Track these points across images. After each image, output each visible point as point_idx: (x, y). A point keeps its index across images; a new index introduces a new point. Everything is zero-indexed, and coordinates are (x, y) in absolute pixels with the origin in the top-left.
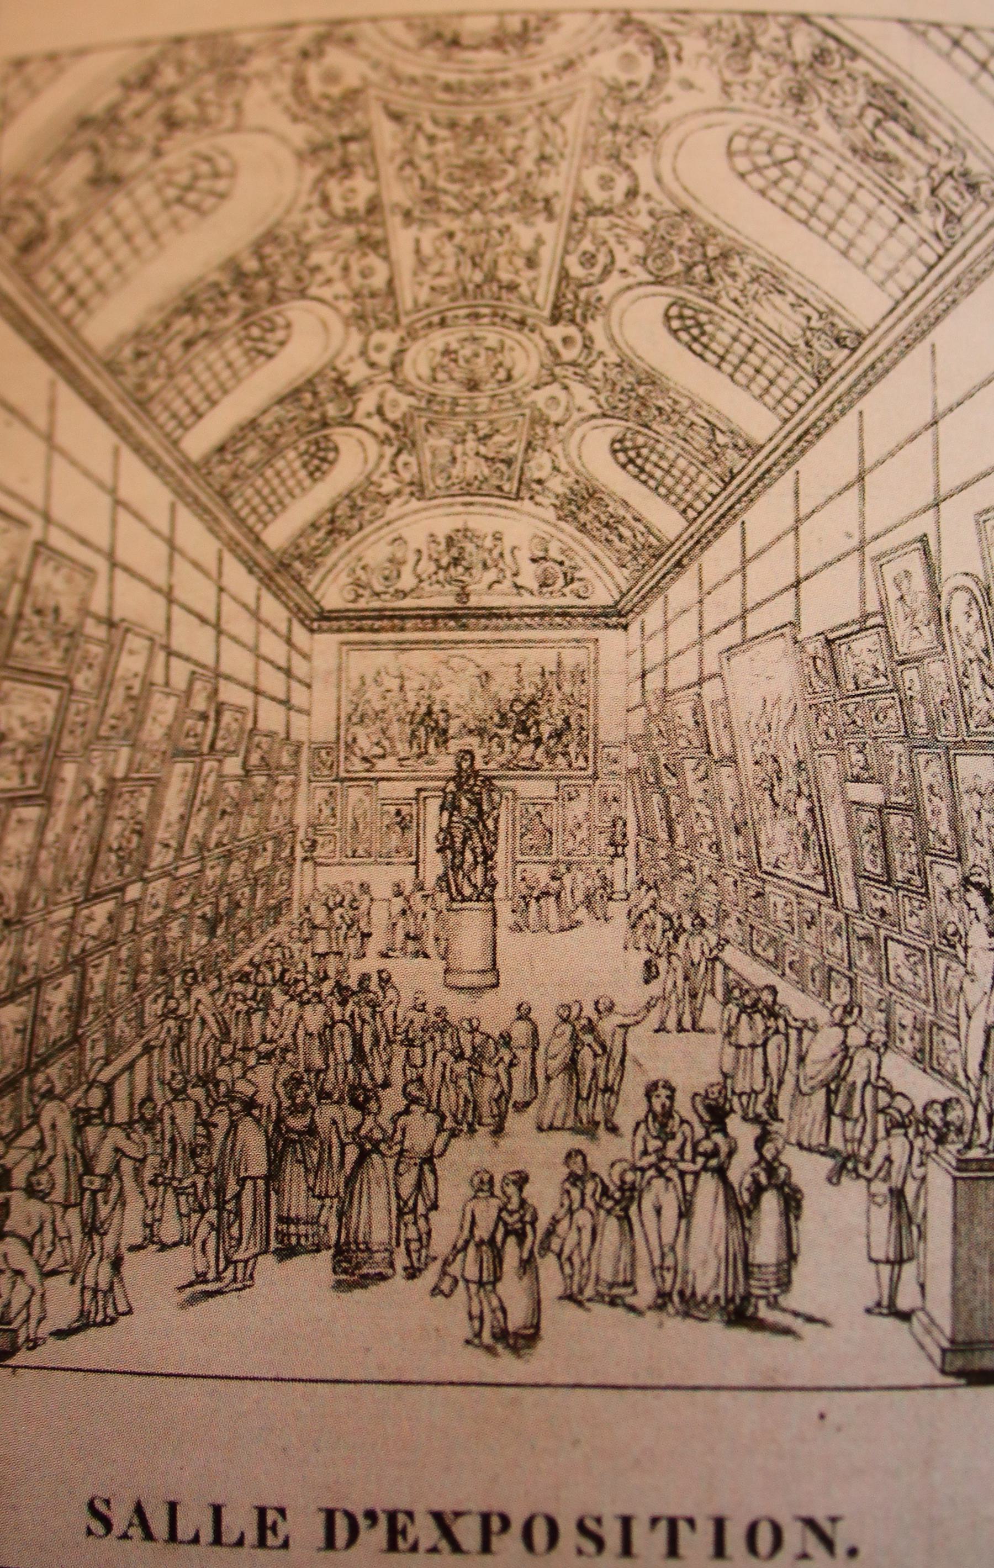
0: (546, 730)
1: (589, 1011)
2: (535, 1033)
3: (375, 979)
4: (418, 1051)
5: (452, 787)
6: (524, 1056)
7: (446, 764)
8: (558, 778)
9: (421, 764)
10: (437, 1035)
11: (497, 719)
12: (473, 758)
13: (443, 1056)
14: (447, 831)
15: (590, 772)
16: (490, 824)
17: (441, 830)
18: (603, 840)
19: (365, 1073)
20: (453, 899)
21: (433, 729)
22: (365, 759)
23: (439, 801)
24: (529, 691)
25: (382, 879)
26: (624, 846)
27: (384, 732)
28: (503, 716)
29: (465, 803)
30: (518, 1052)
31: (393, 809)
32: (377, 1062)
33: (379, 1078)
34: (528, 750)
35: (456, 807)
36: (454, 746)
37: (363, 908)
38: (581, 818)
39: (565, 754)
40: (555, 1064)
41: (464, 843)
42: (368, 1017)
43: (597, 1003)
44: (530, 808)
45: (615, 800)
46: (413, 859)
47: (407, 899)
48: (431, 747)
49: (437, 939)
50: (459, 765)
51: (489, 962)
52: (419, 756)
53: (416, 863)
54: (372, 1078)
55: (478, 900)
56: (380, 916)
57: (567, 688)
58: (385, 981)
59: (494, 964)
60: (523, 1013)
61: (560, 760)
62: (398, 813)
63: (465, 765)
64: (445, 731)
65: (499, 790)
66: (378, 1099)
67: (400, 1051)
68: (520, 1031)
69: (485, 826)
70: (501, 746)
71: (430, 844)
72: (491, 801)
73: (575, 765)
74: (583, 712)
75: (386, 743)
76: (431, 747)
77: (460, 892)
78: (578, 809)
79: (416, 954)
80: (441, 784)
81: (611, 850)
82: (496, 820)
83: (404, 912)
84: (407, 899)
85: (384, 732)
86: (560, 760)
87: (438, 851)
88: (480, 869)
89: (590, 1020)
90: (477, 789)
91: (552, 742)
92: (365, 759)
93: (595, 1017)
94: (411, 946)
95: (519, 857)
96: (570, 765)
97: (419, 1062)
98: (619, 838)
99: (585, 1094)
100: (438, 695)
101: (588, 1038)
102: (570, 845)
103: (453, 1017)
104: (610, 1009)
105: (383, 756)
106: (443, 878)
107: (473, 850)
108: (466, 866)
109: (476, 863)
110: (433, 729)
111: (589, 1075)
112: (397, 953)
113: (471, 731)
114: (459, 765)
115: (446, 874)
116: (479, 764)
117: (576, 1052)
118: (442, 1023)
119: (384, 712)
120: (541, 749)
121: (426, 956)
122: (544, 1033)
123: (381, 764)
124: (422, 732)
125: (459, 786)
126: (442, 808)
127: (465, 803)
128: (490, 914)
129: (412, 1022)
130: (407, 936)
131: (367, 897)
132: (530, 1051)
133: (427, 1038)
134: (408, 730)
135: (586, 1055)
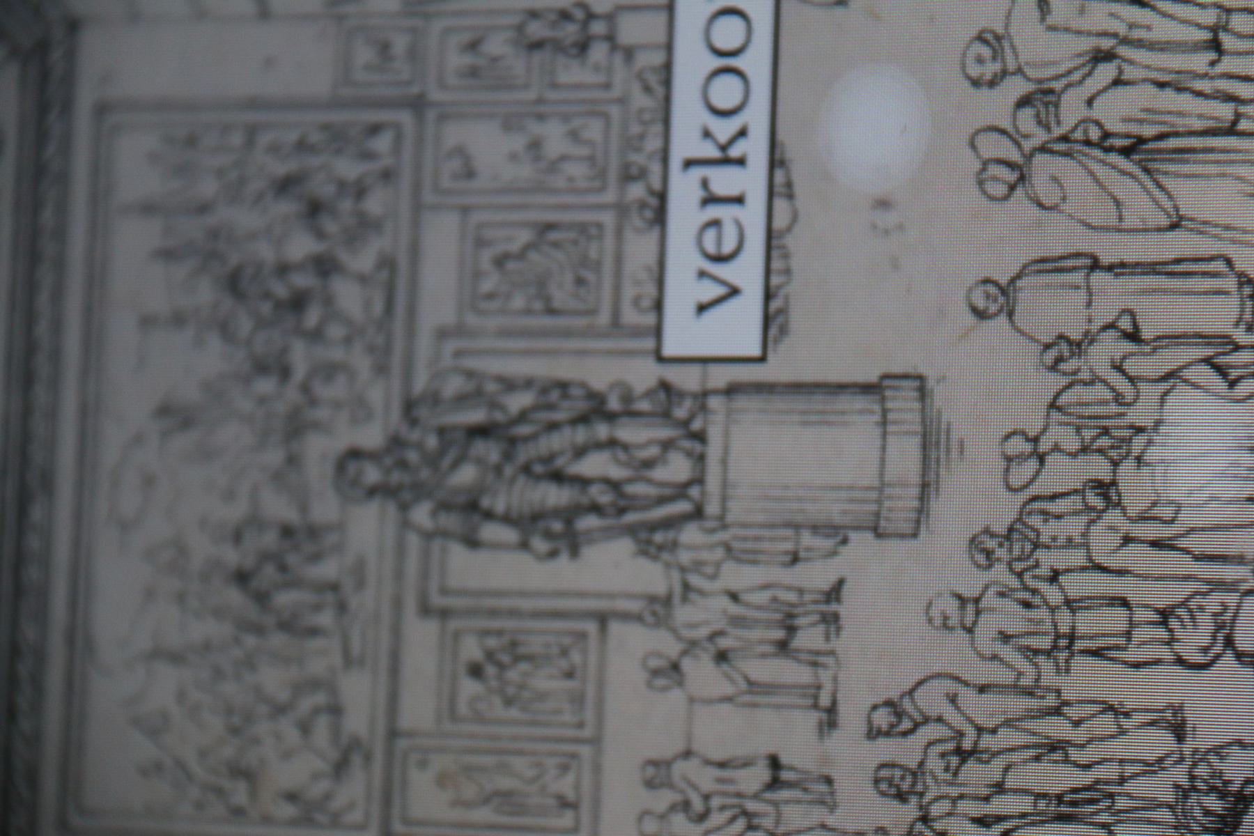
0: (301, 246)
1: (997, 105)
2: (1048, 265)
3: (887, 749)
4: (1086, 623)
5: (422, 514)
6: (1113, 295)
7: (368, 527)
8: (418, 208)
9: (363, 602)
10: (1048, 560)
11: (266, 385)
12: (355, 454)
13: (1103, 543)
14: (528, 522)
15: (405, 118)
16: (518, 402)
17: (524, 545)
18: (571, 73)
19: (1142, 787)
20: (698, 513)
21: (283, 568)
22: (340, 768)
23: (458, 555)
24: (206, 293)
25: (640, 719)
26: (591, 16)
27: (280, 710)
28: (261, 368)
29: (466, 475)
30: (1105, 311)
31: (469, 687)
32: (1117, 748)
33: (1159, 742)
34: (348, 296)
35: (472, 507)
36: (325, 508)
37: (707, 779)
38: (518, 142)
39: (360, 191)
40: (1140, 204)
41: (558, 477)
42: (994, 771)
43: (976, 83)
44: (487, 286)
45: (473, 46)
46: (591, 627)
47: (691, 646)
48: (328, 569)
49: (795, 559)
50: (372, 492)
51: (860, 402)
52: (342, 608)
53: (603, 619)
54: (1155, 766)
55: (701, 437)
56: (731, 731)
57: (208, 188)
58: (897, 717)
59: (867, 389)
60: (998, 299)
61: (374, 204)
62: (476, 671)
63: (372, 475)
64: (287, 532)
65: (438, 376)
66: (1218, 751)
67: (1087, 679)
68: (1054, 308)
69: (523, 417)
70: (329, 371)
71: (564, 574)
72: (462, 400)
73: (387, 161)
74: (264, 139)
75: (307, 703)
76: (328, 569)
77: (680, 491)
78: (491, 147)
79: (831, 621)
80: (413, 540)
81: (598, 52)
82: (510, 385)
83: (722, 657)
84: (691, 646)
85: (280, 710)
86: (374, 204)
87: (575, 552)
88: (628, 432)
89: (1024, 102)
90: (432, 442)
91: (331, 226)
92: (340, 768)
93: (1016, 88)
94: (809, 637)
95: (604, 318)
96: (387, 176)
97: (1115, 619)
98: (570, 31)
99: (1225, 111)
100: (202, 548)
101: (1071, 111)
102: (578, 171)
103: (1003, 511)
104: (992, 40)
105: (335, 711)
106: (647, 549)
107: (580, 452)
108: (616, 473)
109: (612, 443)
110: (283, 568)
111: (1169, 100)
112: (825, 677)
113: (293, 461)
114: (372, 492)
115: (631, 530)
116: (371, 437)
117: (1104, 142)
118: (1011, 545)
119: (229, 711)
120: (343, 256)
121: (835, 593)
122: (1061, 238)
123: (356, 722)
124: (285, 599)
125: (420, 491)
126: (473, 543)
127: (466, 475)
128: (741, 402)
129: (1005, 637)
130: (783, 647)
131: (679, 768)
132: (1098, 278)
133: (1053, 595)
134: (278, 640)
135: (1117, 111)
